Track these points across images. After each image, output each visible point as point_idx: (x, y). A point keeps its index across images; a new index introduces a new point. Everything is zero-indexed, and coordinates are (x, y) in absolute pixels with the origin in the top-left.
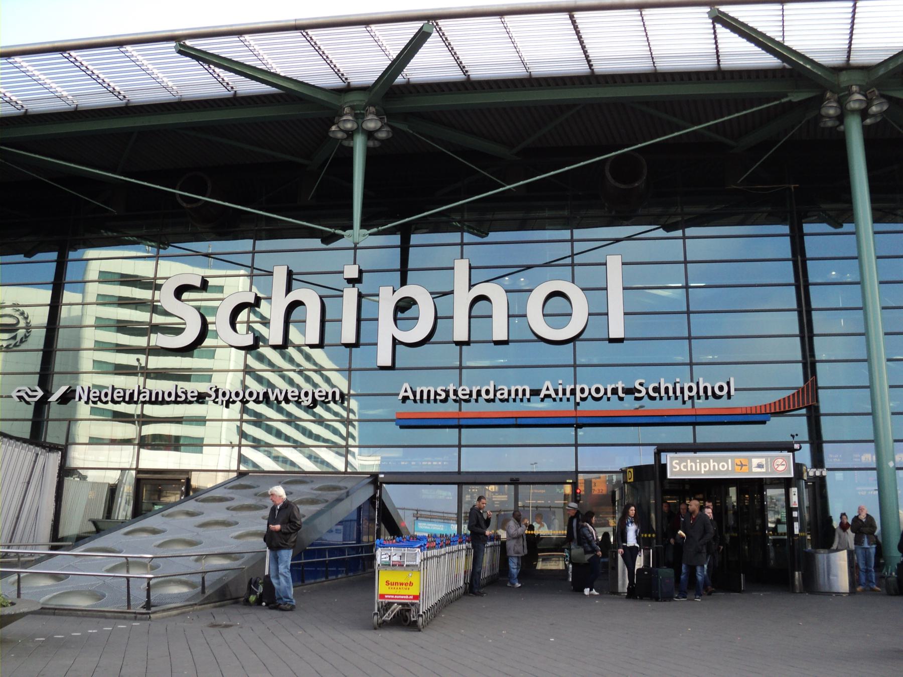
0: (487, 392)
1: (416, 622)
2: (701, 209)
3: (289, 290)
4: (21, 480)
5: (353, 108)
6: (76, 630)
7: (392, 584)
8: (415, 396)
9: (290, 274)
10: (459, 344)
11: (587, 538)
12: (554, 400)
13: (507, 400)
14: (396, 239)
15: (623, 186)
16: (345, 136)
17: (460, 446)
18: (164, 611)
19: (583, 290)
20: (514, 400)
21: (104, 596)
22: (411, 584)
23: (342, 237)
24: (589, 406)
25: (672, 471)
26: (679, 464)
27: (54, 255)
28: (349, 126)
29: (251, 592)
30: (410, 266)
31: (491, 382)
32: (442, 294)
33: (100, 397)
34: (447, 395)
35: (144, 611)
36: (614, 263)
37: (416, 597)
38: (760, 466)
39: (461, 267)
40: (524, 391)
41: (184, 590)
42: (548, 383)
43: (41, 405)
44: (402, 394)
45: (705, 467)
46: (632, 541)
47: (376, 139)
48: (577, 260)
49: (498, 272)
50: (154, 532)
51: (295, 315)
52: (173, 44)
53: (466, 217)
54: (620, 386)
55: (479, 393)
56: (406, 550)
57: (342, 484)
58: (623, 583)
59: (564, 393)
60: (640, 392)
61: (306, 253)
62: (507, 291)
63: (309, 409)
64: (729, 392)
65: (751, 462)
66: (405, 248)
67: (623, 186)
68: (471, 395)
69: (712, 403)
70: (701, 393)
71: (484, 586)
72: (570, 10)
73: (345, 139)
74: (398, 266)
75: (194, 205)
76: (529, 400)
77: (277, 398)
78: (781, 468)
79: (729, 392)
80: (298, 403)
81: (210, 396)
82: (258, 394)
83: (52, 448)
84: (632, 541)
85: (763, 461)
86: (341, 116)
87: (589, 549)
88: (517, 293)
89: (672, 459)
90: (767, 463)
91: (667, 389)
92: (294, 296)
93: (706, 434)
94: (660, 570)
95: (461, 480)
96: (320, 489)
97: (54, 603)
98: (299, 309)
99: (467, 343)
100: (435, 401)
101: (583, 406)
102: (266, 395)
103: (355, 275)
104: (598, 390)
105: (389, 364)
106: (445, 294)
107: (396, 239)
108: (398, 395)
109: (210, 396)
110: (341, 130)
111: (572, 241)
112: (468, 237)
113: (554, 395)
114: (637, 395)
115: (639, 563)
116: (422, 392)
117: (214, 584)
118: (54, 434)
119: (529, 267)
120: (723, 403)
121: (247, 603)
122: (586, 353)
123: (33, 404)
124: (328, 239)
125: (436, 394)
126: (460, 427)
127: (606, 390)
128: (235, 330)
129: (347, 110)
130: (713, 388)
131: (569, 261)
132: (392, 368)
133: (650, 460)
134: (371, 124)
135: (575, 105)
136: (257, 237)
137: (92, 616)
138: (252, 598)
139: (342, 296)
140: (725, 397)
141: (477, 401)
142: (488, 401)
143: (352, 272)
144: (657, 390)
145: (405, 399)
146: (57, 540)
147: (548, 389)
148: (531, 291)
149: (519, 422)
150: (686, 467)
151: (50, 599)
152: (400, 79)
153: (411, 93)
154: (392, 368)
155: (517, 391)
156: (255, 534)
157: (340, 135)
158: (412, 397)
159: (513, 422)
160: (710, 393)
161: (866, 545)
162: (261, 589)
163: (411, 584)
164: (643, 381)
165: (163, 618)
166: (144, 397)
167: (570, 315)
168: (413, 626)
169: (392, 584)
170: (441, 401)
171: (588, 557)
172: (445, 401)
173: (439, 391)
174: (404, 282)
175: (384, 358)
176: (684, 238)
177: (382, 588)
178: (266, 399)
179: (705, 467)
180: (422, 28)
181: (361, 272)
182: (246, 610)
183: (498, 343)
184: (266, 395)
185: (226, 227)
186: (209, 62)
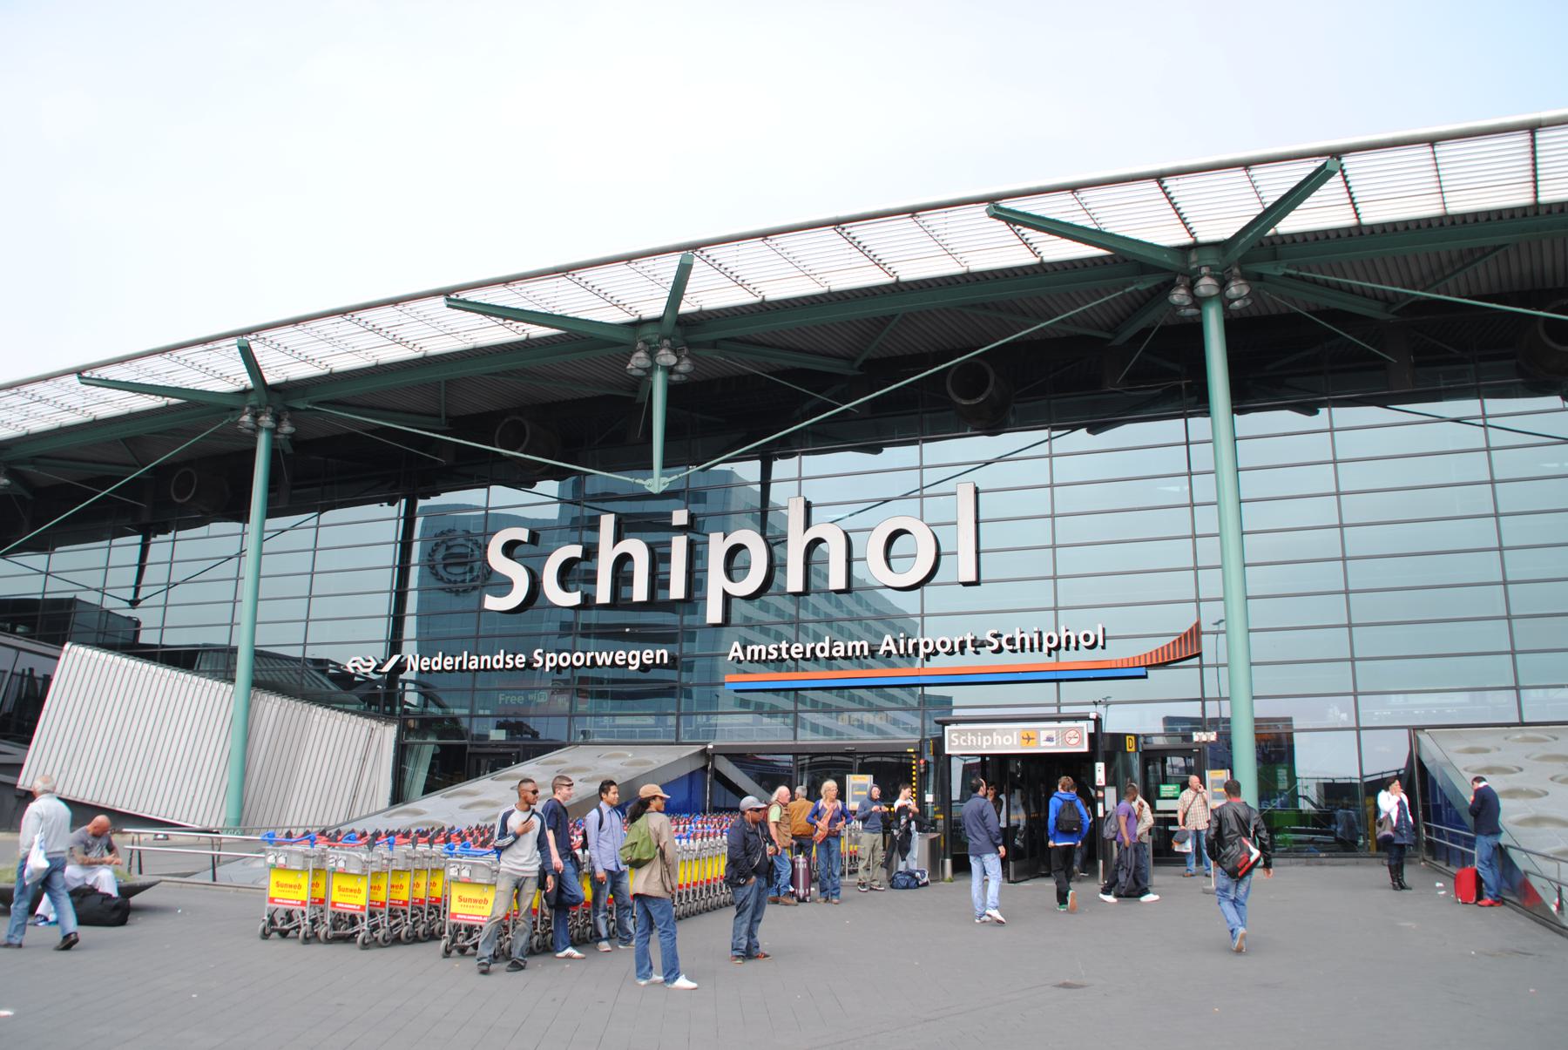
4: (358, 756)
9: (808, 506)
27: (138, 539)
38: (1049, 739)
48: (926, 491)
69: (1084, 656)
72: (1159, 177)
78: (1074, 741)
85: (1053, 734)
92: (813, 533)
125: (768, 653)
126: (1058, 681)
129: (640, 345)
144: (1011, 641)
175: (714, 614)
180: (1324, 165)
183: (965, 584)
186: (1016, 223)
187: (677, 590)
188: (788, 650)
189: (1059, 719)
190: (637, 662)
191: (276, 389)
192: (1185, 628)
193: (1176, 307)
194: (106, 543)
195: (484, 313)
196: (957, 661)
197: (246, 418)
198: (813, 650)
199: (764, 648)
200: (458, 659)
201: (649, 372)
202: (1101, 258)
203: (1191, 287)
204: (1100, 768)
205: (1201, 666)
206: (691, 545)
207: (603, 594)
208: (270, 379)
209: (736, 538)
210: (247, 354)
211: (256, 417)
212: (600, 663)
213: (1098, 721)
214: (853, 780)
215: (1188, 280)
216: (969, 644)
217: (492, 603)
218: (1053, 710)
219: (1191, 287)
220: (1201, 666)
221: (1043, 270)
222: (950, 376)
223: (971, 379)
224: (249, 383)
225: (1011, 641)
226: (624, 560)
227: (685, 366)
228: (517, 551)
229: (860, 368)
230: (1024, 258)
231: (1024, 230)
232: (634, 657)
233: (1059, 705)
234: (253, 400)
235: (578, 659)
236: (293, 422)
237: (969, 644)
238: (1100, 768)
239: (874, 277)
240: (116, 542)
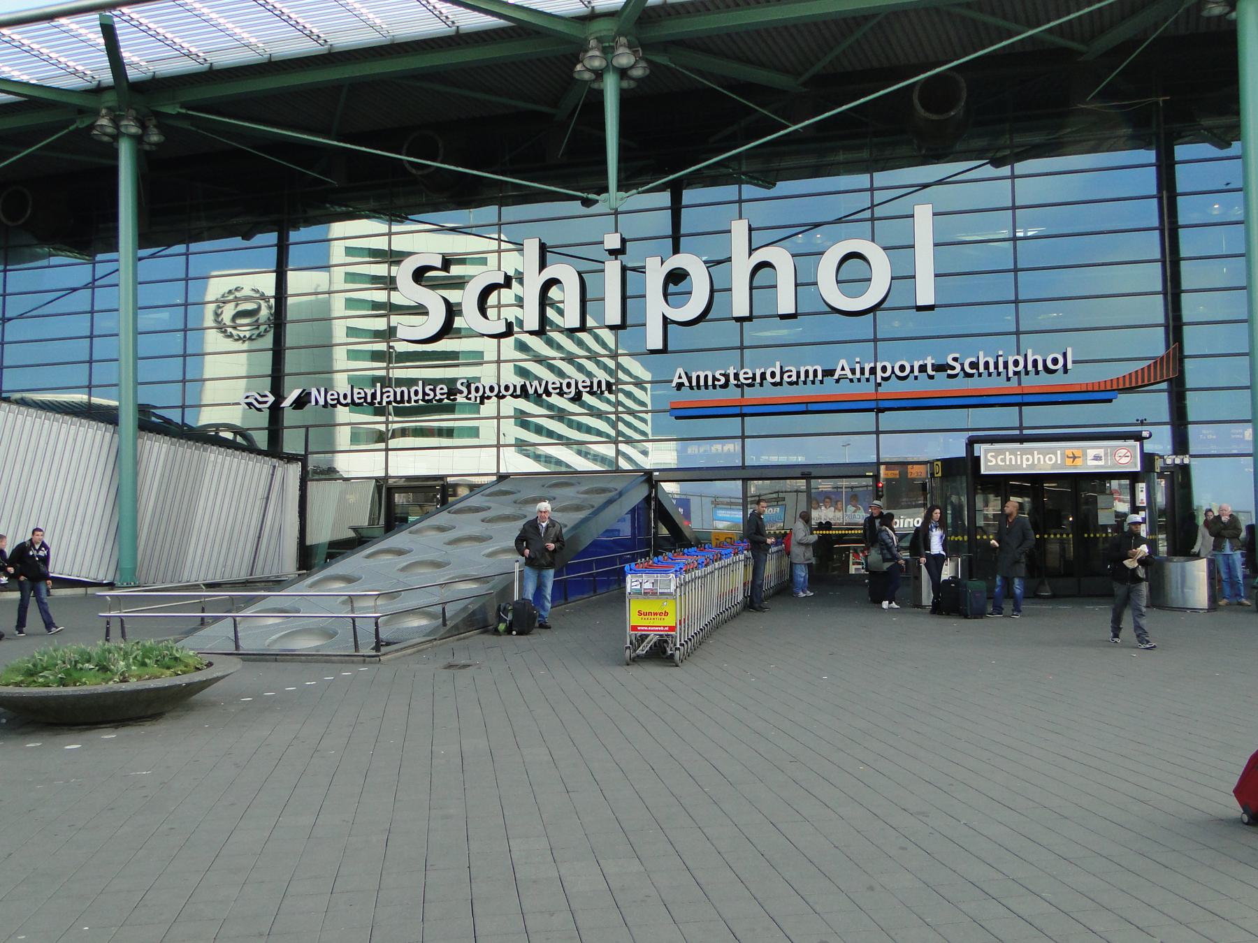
0: (773, 375)
1: (672, 655)
2: (1037, 139)
3: (543, 265)
4: (259, 496)
5: (600, 40)
6: (288, 681)
7: (645, 614)
8: (690, 382)
9: (543, 249)
10: (740, 320)
11: (886, 544)
12: (851, 380)
13: (796, 383)
14: (665, 198)
15: (935, 117)
16: (593, 76)
17: (743, 437)
18: (397, 651)
19: (885, 249)
20: (805, 383)
21: (336, 633)
22: (666, 614)
23: (597, 201)
25: (987, 467)
26: (995, 457)
27: (272, 237)
28: (597, 63)
29: (501, 620)
30: (683, 231)
31: (777, 366)
32: (718, 263)
33: (338, 399)
34: (727, 381)
35: (374, 653)
36: (923, 216)
37: (672, 629)
38: (1097, 458)
39: (739, 230)
40: (815, 372)
41: (423, 622)
42: (843, 362)
43: (276, 410)
44: (676, 380)
45: (1028, 460)
46: (936, 547)
47: (633, 79)
48: (878, 212)
49: (784, 233)
50: (400, 552)
53: (744, 169)
54: (929, 362)
55: (763, 376)
56: (659, 577)
57: (611, 485)
58: (927, 597)
59: (862, 372)
60: (953, 368)
61: (564, 218)
62: (793, 256)
63: (577, 398)
64: (1065, 365)
65: (1085, 455)
66: (676, 208)
67: (935, 117)
68: (754, 378)
69: (1044, 380)
70: (1030, 367)
71: (769, 597)
73: (594, 81)
74: (669, 231)
75: (425, 172)
76: (822, 382)
77: (536, 390)
79: (1065, 365)
80: (561, 394)
81: (461, 392)
82: (515, 387)
83: (291, 458)
84: (936, 547)
85: (1101, 452)
86: (586, 51)
87: (889, 556)
88: (807, 257)
89: (987, 451)
90: (1106, 454)
91: (987, 364)
92: (549, 273)
93: (1036, 416)
94: (969, 583)
95: (746, 474)
96: (586, 492)
97: (276, 648)
99: (749, 319)
100: (714, 386)
101: (886, 388)
102: (523, 387)
103: (618, 245)
104: (902, 368)
105: (660, 346)
106: (719, 262)
107: (665, 198)
108: (671, 381)
109: (461, 392)
110: (588, 70)
111: (872, 189)
112: (749, 190)
113: (850, 376)
114: (950, 372)
115: (947, 572)
116: (698, 377)
117: (456, 614)
118: (292, 442)
120: (1058, 379)
121: (496, 632)
122: (889, 324)
123: (267, 411)
124: (587, 203)
125: (714, 379)
127: (912, 367)
128: (486, 318)
129: (593, 43)
130: (1045, 361)
131: (867, 214)
132: (664, 351)
133: (959, 451)
134: (624, 58)
135: (874, 16)
136: (503, 202)
137: (317, 662)
138: (502, 627)
139: (603, 271)
140: (1061, 371)
141: (761, 385)
142: (774, 384)
143: (613, 242)
144: (974, 365)
145: (680, 386)
146: (307, 558)
147: (843, 369)
148: (822, 253)
149: (811, 407)
150: (1003, 460)
151: (275, 641)
153: (669, 15)
154: (664, 351)
155: (807, 372)
156: (505, 551)
157: (587, 76)
158: (687, 384)
159: (803, 408)
160: (1040, 367)
161: (1228, 551)
162: (510, 617)
163: (666, 614)
164: (957, 355)
165: (397, 658)
166: (790, 377)
167: (870, 280)
168: (670, 660)
169: (645, 614)
170: (721, 386)
171: (887, 565)
172: (725, 386)
173: (718, 376)
174: (676, 250)
176: (1013, 177)
177: (634, 619)
178: (524, 394)
179: (1028, 460)
181: (623, 241)
182: (490, 639)
183: (783, 317)
184: (523, 387)
185: (463, 194)
194: (180, 248)
208: (132, 74)
211: (116, 121)
214: (1015, 500)
222: (917, 88)
224: (107, 77)
229: (804, 84)
236: (161, 128)
240: (194, 247)
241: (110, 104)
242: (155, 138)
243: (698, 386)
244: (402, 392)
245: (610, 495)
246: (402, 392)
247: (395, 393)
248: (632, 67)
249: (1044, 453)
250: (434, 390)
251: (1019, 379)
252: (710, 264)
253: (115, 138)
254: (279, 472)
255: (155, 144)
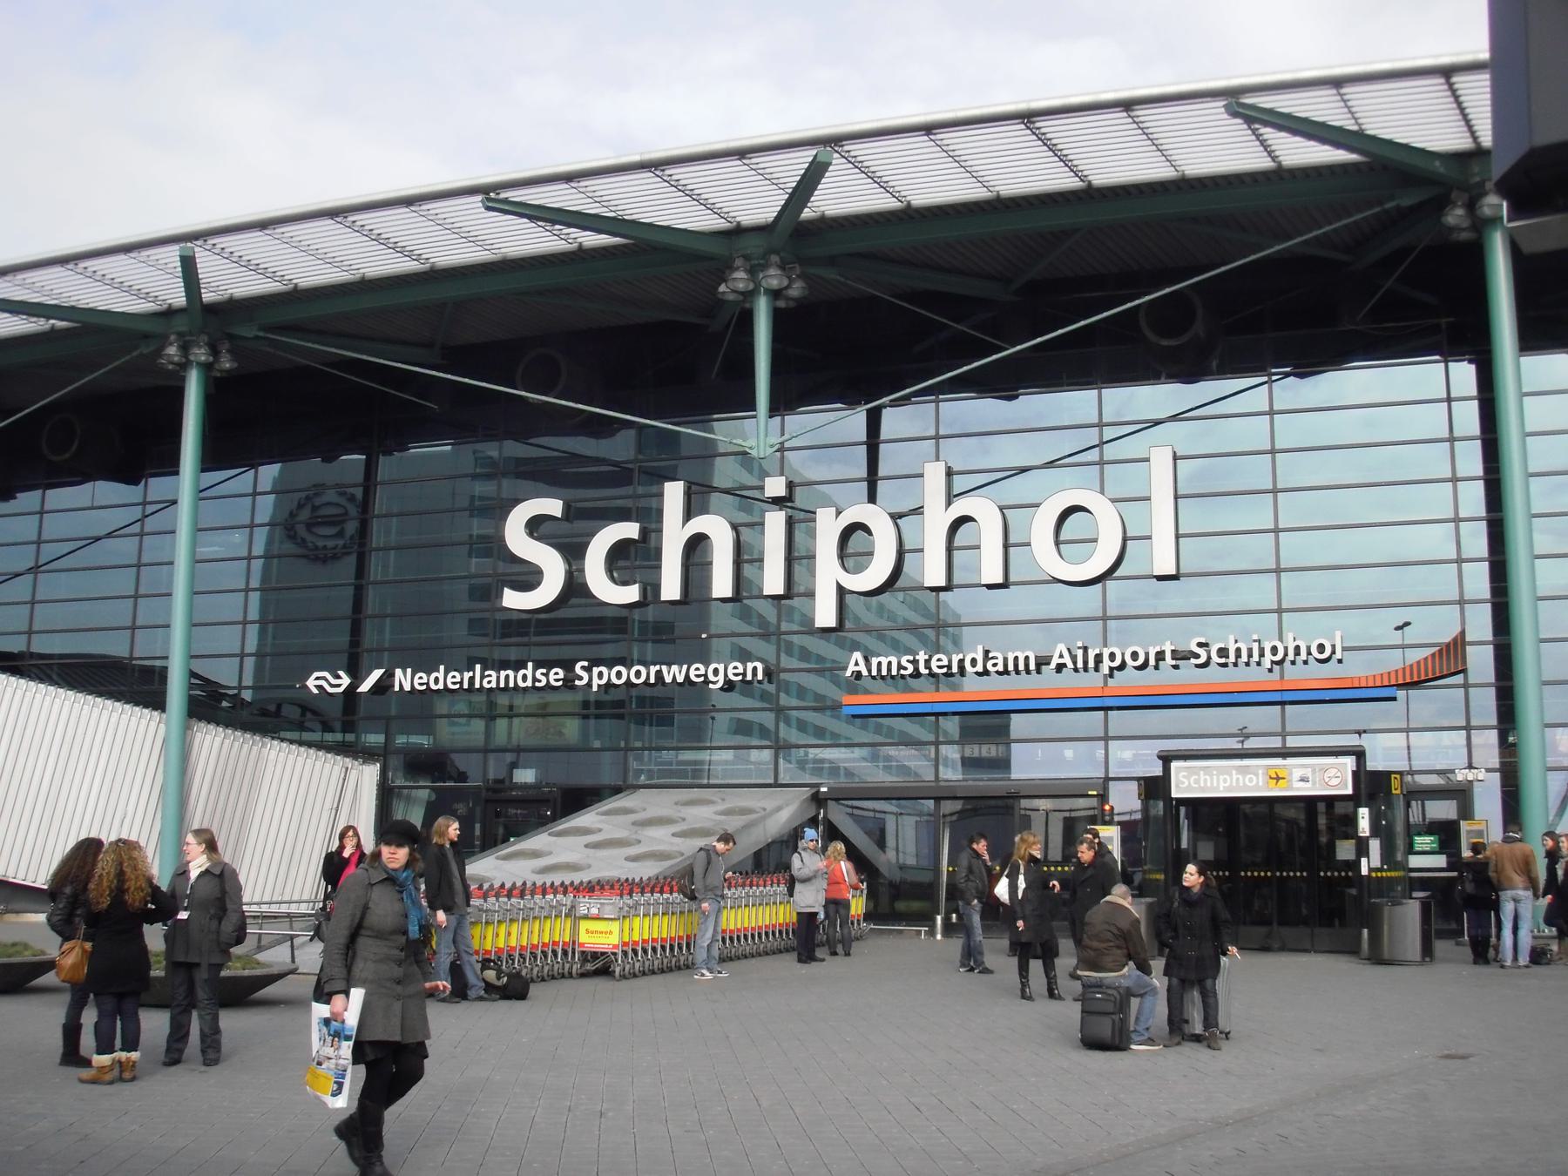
0: (974, 662)
4: (328, 805)
8: (1075, 663)
19: (1113, 501)
24: (1130, 680)
26: (1187, 777)
33: (706, 676)
39: (934, 475)
44: (1055, 661)
48: (1110, 451)
51: (959, 540)
52: (479, 198)
65: (1291, 774)
78: (1334, 782)
85: (1308, 773)
92: (961, 508)
98: (860, 533)
104: (1321, 648)
116: (1016, 658)
119: (1024, 470)
125: (900, 667)
126: (1282, 703)
141: (1156, 667)
144: (1223, 652)
145: (1060, 668)
147: (1061, 656)
148: (1038, 505)
152: (807, 214)
157: (731, 297)
158: (1070, 665)
166: (995, 665)
173: (904, 663)
175: (825, 615)
181: (790, 486)
183: (990, 587)
186: (554, 222)
187: (773, 582)
188: (928, 662)
189: (1285, 753)
190: (721, 677)
191: (213, 309)
192: (1447, 638)
193: (1451, 229)
195: (531, 218)
196: (1149, 679)
197: (172, 350)
198: (961, 662)
199: (894, 660)
200: (467, 675)
201: (750, 295)
202: (615, 247)
203: (1471, 206)
204: (1364, 813)
205: (1466, 686)
206: (790, 523)
207: (671, 588)
208: (208, 296)
209: (852, 515)
210: (189, 266)
211: (185, 348)
212: (668, 679)
213: (1360, 755)
215: (1466, 196)
216: (1168, 655)
217: (513, 600)
218: (1275, 743)
219: (1471, 206)
220: (1466, 686)
221: (1280, 176)
223: (1172, 315)
224: (178, 298)
225: (1223, 652)
226: (696, 546)
227: (797, 290)
228: (545, 528)
230: (1256, 161)
231: (1263, 130)
232: (716, 672)
233: (1284, 734)
234: (181, 324)
235: (638, 674)
237: (1168, 655)
238: (1364, 813)
239: (1157, 171)
241: (181, 329)
242: (227, 365)
243: (1028, 671)
244: (507, 677)
245: (754, 816)
246: (507, 677)
247: (1005, 660)
248: (786, 288)
249: (1244, 771)
250: (546, 675)
251: (1282, 671)
252: (896, 517)
253: (184, 366)
254: (353, 775)
255: (228, 371)
